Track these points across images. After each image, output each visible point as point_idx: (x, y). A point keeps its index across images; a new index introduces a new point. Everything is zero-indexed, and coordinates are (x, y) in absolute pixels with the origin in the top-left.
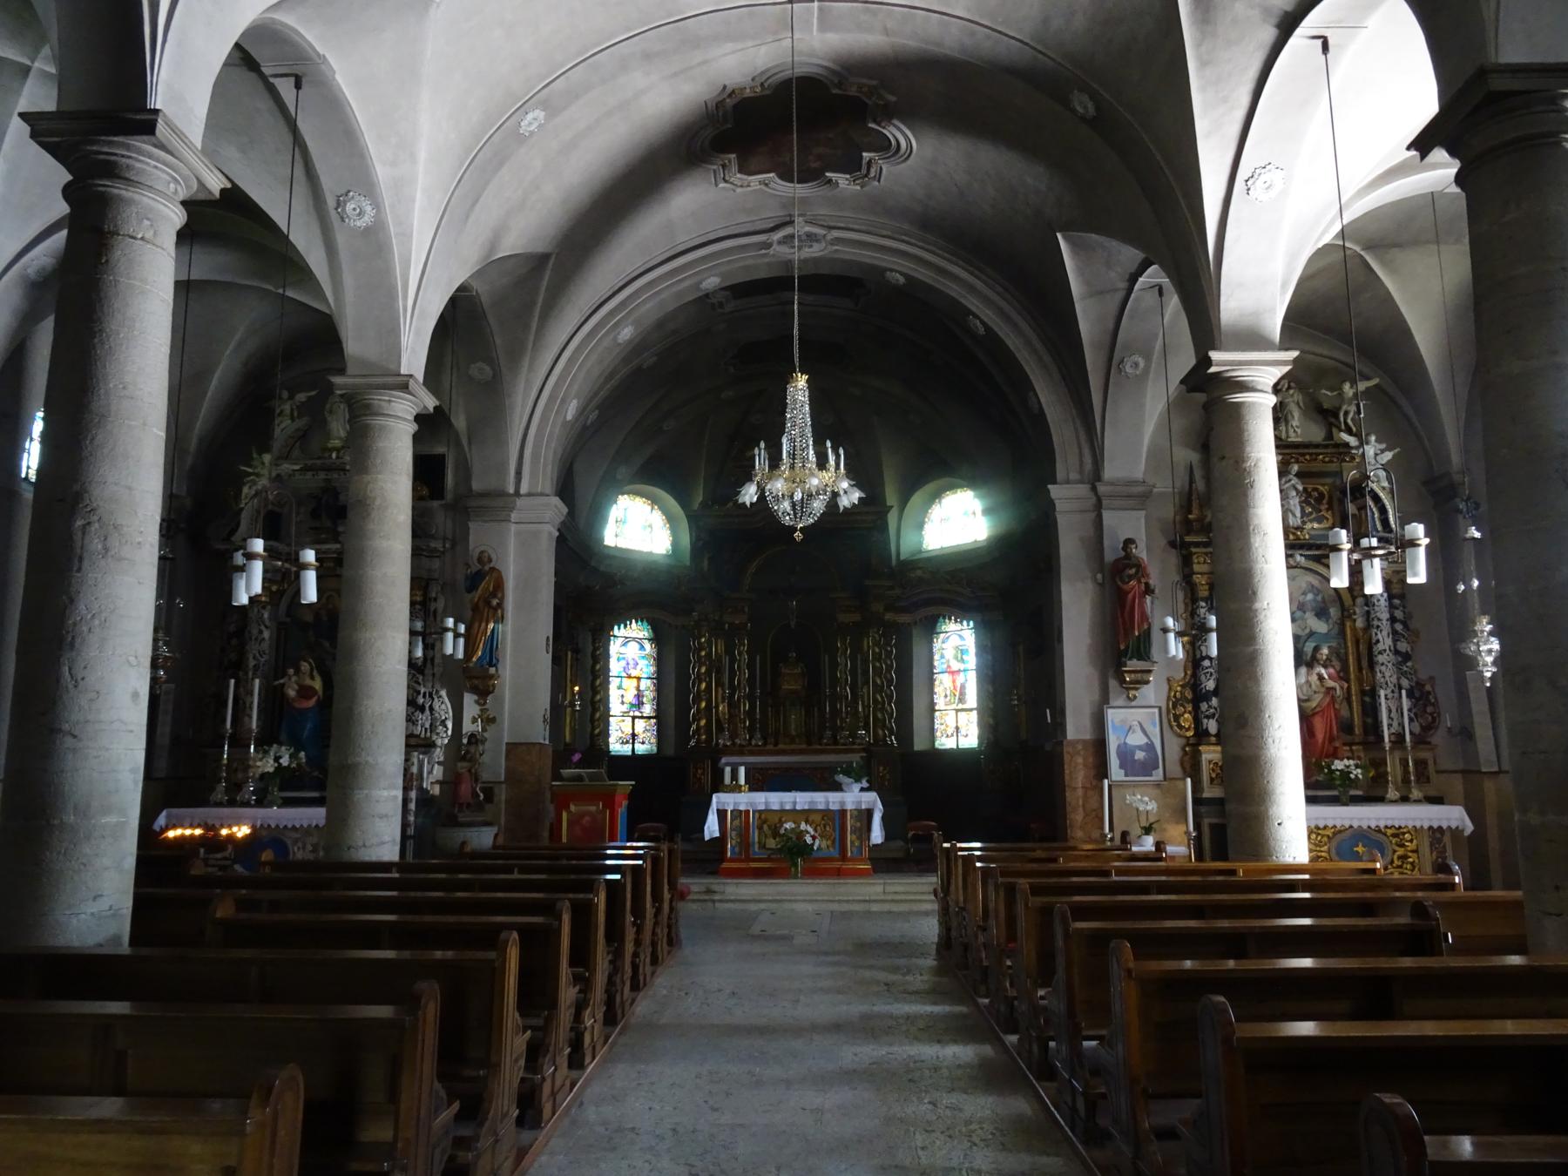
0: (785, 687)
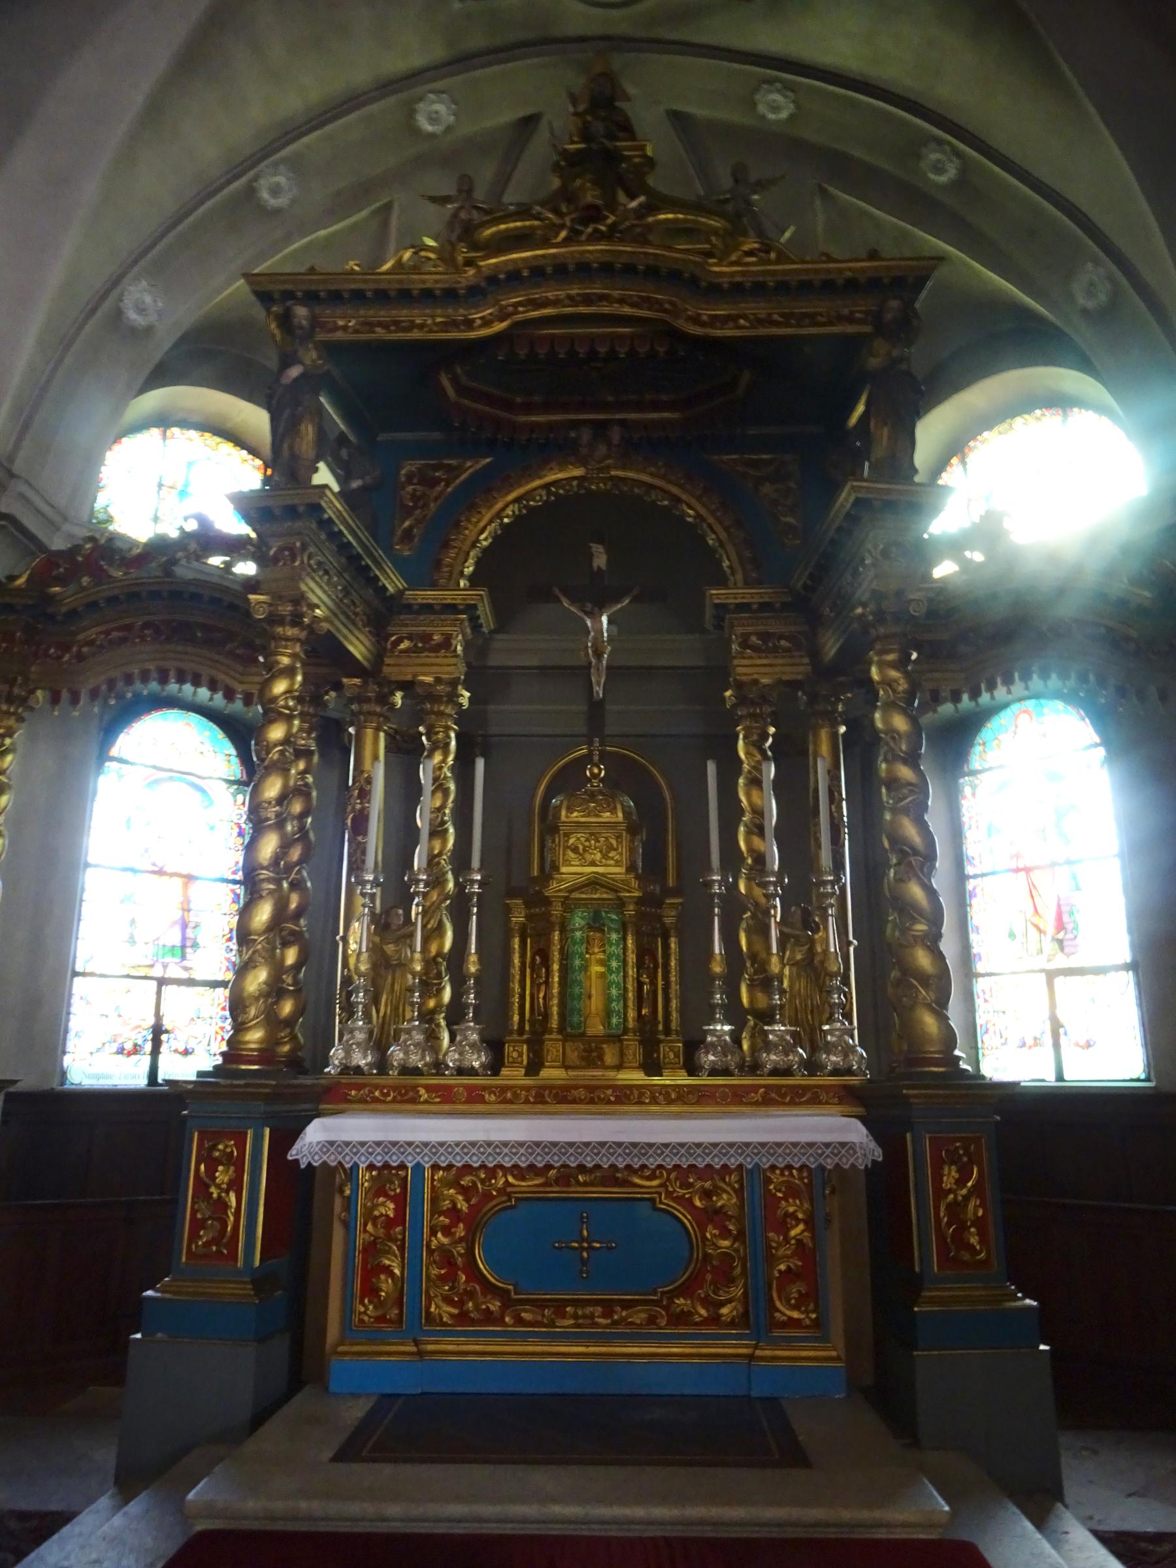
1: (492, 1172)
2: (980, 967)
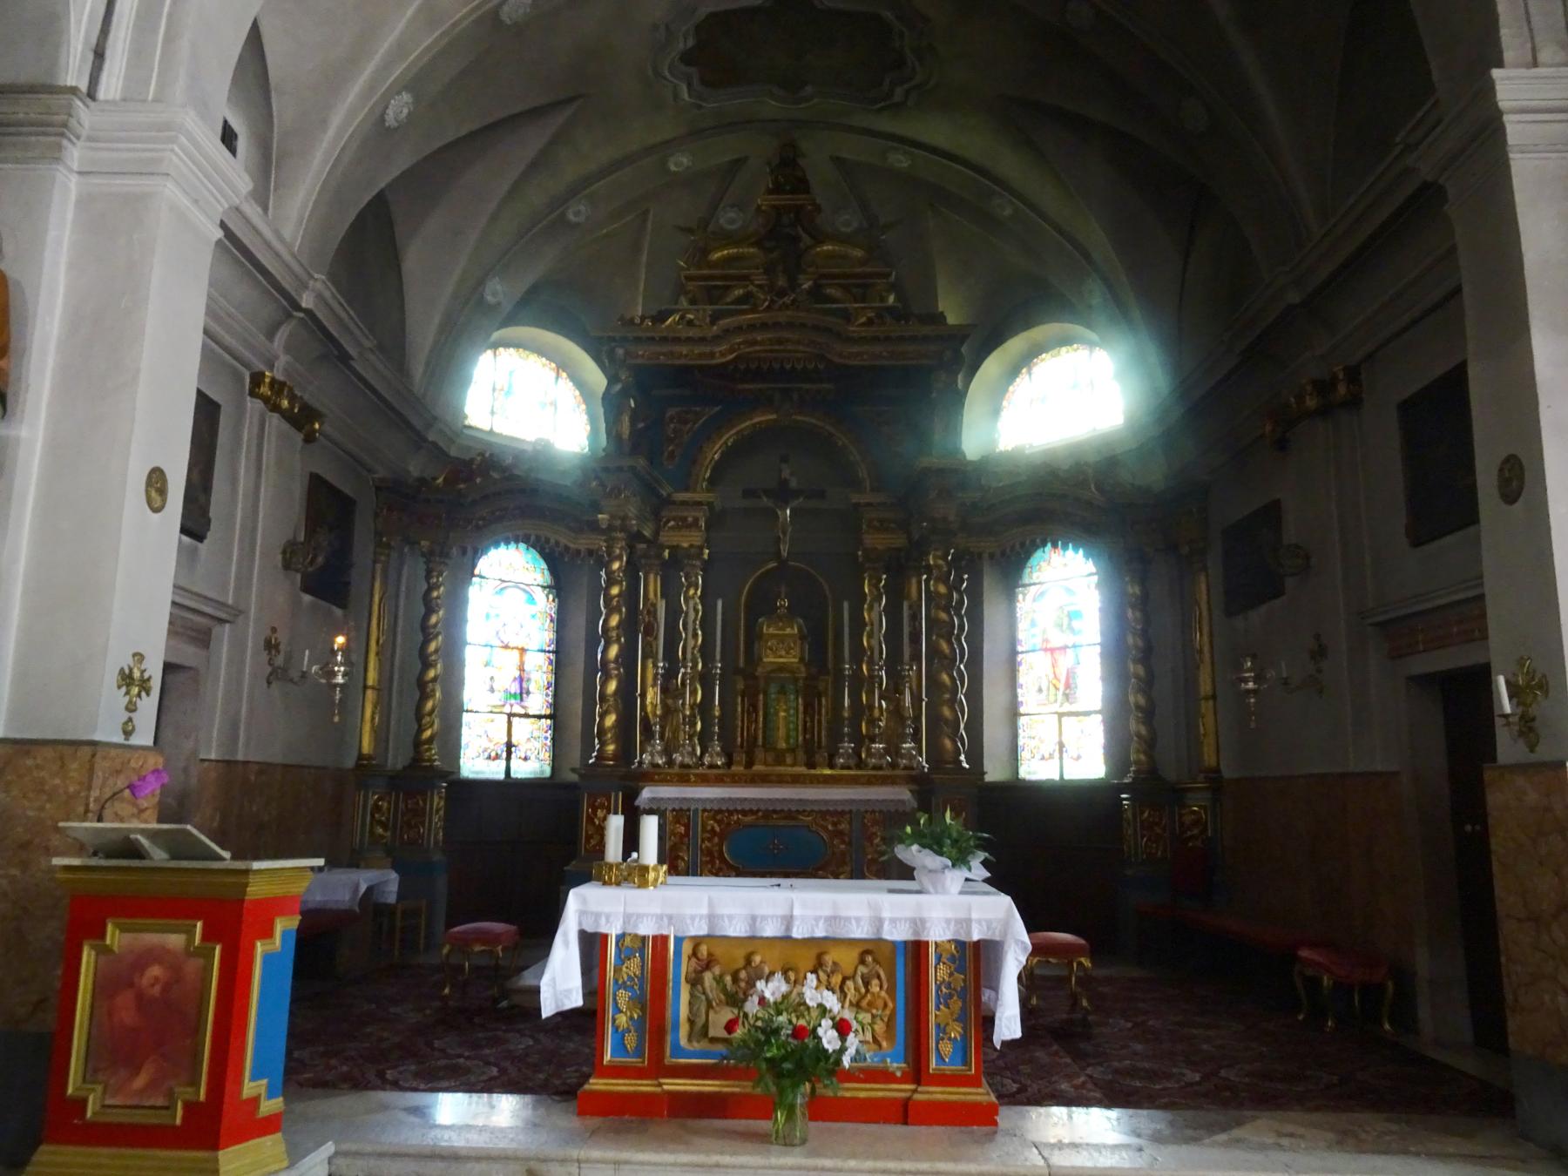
0: (769, 659)
1: (731, 813)
2: (1022, 710)
